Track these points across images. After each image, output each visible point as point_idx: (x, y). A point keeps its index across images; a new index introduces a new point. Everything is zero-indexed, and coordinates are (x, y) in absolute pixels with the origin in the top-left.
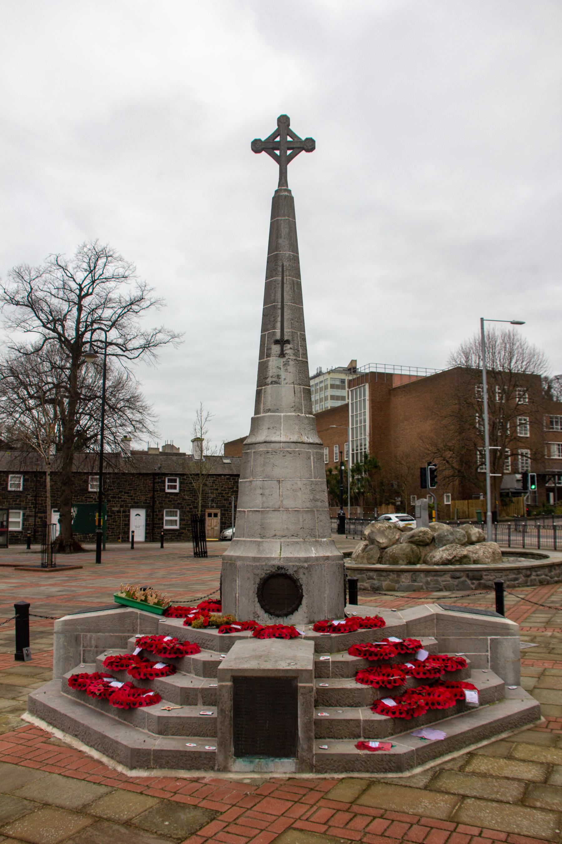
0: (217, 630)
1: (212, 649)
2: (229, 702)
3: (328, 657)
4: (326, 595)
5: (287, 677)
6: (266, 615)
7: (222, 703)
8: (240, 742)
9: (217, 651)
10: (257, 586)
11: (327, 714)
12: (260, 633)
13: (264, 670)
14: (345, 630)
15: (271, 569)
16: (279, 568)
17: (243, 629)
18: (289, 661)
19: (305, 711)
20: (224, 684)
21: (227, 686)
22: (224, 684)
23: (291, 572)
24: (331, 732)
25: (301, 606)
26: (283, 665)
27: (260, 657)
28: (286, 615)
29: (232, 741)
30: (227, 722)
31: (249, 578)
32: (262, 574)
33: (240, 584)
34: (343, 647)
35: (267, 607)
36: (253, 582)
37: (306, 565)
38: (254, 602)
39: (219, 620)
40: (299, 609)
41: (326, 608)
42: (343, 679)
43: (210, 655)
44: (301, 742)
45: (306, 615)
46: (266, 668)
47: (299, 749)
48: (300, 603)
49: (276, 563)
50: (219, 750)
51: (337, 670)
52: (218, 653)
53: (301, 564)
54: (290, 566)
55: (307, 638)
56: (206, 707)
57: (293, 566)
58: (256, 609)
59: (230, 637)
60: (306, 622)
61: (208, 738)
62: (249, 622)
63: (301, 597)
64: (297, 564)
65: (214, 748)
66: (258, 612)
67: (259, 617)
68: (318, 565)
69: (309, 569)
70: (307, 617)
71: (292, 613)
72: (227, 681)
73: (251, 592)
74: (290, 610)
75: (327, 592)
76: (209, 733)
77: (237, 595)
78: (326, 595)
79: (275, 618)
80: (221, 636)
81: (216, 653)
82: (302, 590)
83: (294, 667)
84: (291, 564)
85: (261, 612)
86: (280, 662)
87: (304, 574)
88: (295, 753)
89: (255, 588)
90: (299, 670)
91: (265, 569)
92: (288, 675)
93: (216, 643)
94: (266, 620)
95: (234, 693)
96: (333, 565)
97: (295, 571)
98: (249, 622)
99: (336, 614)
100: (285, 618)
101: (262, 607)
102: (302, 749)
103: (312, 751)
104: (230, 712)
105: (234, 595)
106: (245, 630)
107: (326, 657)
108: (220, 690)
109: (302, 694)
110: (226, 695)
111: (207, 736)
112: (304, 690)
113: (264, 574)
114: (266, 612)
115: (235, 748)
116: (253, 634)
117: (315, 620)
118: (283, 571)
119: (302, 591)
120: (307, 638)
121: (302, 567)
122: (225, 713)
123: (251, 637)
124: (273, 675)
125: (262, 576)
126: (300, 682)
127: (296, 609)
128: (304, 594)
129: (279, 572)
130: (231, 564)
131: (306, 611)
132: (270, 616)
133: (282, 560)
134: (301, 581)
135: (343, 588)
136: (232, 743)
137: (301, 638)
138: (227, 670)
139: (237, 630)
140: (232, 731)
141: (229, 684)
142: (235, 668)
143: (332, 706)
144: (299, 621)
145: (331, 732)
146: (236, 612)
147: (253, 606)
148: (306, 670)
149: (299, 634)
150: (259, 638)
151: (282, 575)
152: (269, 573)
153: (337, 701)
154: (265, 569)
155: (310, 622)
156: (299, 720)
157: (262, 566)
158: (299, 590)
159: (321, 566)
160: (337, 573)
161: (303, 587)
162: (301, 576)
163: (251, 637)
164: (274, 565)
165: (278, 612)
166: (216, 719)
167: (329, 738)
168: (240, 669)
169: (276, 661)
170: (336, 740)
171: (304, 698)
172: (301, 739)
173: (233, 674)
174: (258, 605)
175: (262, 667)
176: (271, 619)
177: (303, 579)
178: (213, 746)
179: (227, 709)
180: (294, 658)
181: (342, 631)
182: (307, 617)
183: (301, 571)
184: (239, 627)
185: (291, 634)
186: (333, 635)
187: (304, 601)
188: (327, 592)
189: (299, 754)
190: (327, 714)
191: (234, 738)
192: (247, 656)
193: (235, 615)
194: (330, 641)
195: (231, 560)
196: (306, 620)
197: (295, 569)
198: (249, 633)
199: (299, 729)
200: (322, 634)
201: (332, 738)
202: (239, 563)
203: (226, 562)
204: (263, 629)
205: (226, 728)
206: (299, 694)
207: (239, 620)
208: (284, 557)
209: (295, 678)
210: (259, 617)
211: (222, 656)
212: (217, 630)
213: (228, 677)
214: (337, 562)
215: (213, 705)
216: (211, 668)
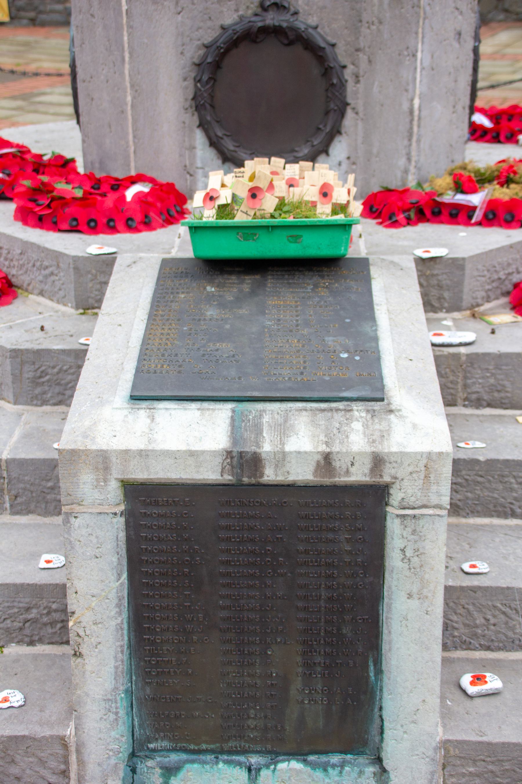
33: (427, 63)
77: (416, 102)
105: (406, 106)
146: (409, 160)
151: (276, 31)
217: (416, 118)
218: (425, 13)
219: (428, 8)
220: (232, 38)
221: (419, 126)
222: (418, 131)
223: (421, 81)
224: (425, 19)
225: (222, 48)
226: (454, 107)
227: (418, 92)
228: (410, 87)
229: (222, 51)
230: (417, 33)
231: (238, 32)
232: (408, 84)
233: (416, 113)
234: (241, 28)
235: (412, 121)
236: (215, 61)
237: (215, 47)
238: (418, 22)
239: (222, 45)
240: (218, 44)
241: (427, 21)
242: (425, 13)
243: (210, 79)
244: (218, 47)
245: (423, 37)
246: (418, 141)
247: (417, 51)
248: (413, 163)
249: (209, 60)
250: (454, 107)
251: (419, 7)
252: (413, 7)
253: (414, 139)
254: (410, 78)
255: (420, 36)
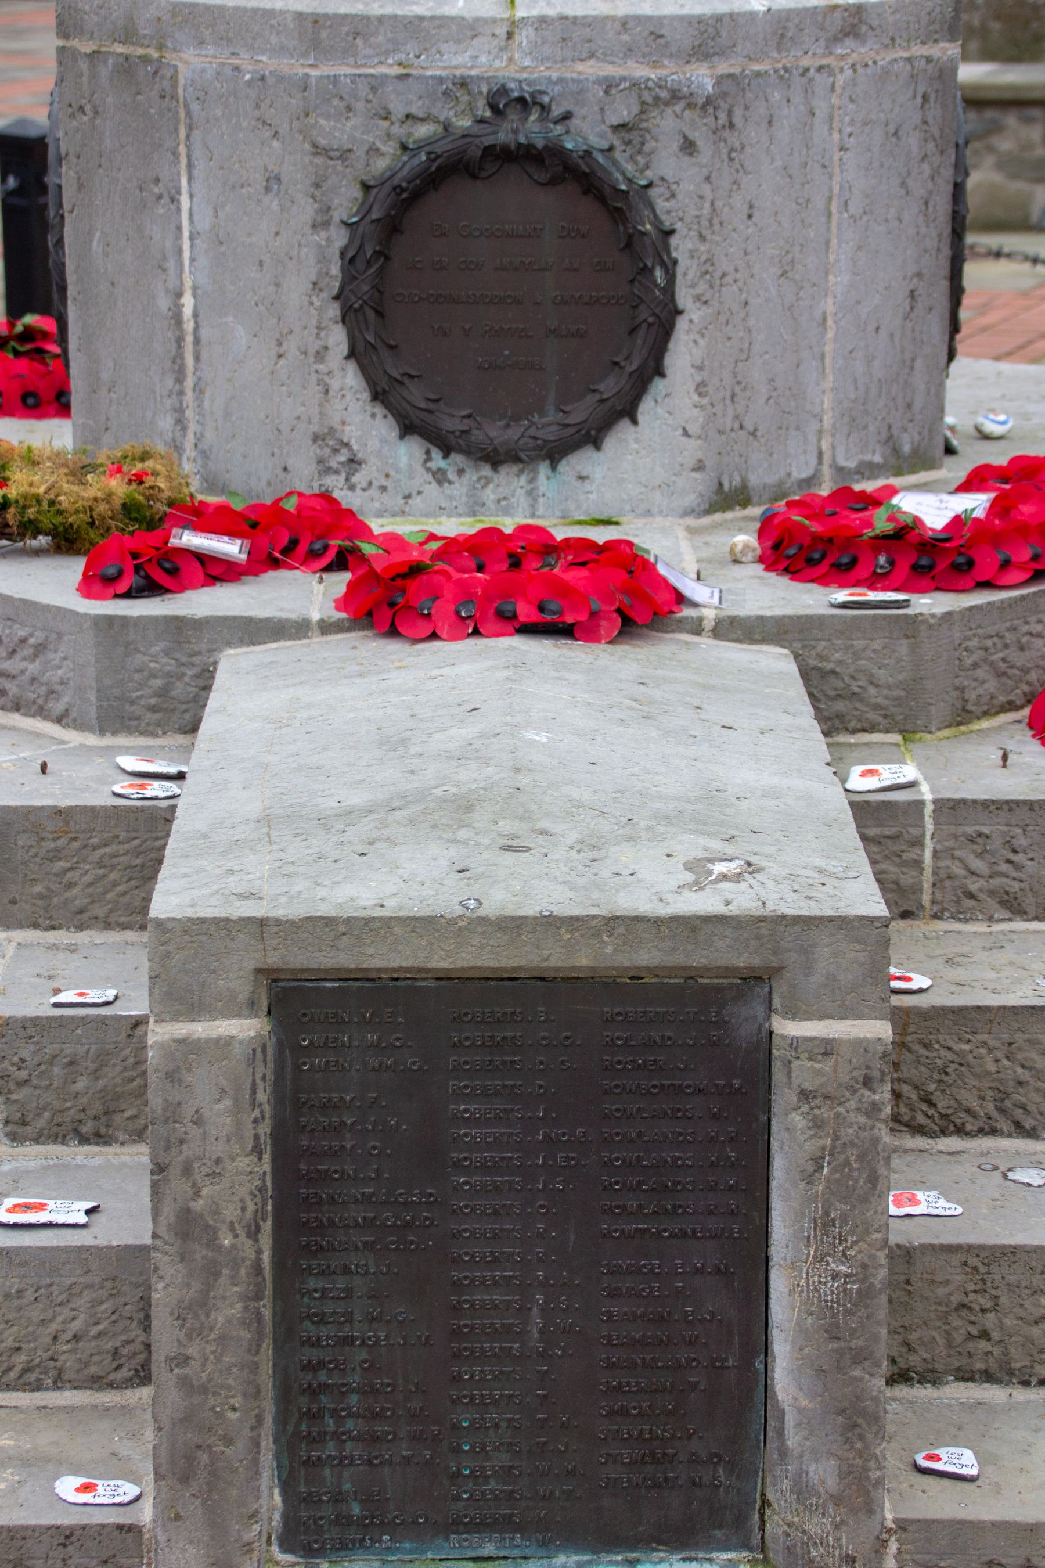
0: (74, 568)
1: (41, 712)
2: (244, 1163)
3: (909, 772)
4: (829, 306)
5: (690, 975)
6: (408, 453)
7: (187, 1171)
8: (331, 1449)
9: (81, 726)
10: (340, 238)
11: (943, 1206)
12: (394, 598)
13: (513, 926)
14: (1006, 565)
15: (445, 112)
16: (505, 102)
17: (262, 562)
18: (690, 845)
19: (826, 1223)
20: (200, 1029)
21: (224, 1044)
22: (200, 1029)
23: (587, 133)
24: (985, 1335)
25: (659, 386)
26: (655, 883)
27: (464, 806)
28: (554, 454)
29: (267, 1443)
30: (229, 1309)
31: (273, 181)
32: (373, 151)
33: (204, 223)
34: (991, 685)
35: (416, 394)
36: (306, 211)
37: (702, 78)
38: (321, 355)
39: (75, 496)
40: (646, 408)
41: (825, 397)
42: (1019, 925)
43: (34, 755)
44: (793, 1440)
45: (692, 450)
46: (530, 910)
47: (779, 1492)
48: (654, 367)
49: (484, 62)
50: (171, 1514)
51: (977, 864)
52: (92, 740)
53: (672, 72)
54: (580, 90)
55: (736, 629)
56: (33, 1156)
57: (609, 86)
58: (337, 405)
59: (179, 627)
60: (690, 499)
61: (68, 1397)
62: (290, 505)
63: (664, 321)
64: (641, 72)
65: (129, 1490)
66: (351, 433)
67: (354, 463)
68: (784, 77)
69: (719, 108)
70: (700, 467)
71: (593, 437)
72: (228, 1015)
73: (296, 288)
74: (580, 412)
75: (839, 280)
76: (69, 1363)
77: (188, 302)
78: (829, 306)
79: (471, 476)
80: (110, 621)
81: (74, 737)
82: (670, 268)
83: (742, 899)
84: (590, 70)
85: (370, 430)
86: (623, 857)
87: (689, 147)
88: (740, 1521)
89: (322, 259)
90: (782, 920)
91: (399, 110)
92: (699, 959)
93: (74, 665)
94: (417, 501)
95: (279, 1098)
96: (886, 74)
97: (621, 127)
98: (290, 505)
99: (891, 442)
100: (544, 468)
101: (378, 395)
102: (802, 1490)
103: (871, 1508)
104: (254, 1233)
105: (163, 303)
106: (275, 564)
107: (890, 774)
108: (172, 1076)
109: (805, 1095)
110: (220, 1114)
111: (59, 1383)
112: (826, 1066)
113: (390, 148)
114: (408, 428)
115: (287, 1486)
116: (344, 603)
117: (754, 480)
118: (532, 130)
119: (671, 278)
120: (736, 629)
121: (675, 96)
122: (212, 1242)
123: (326, 628)
124: (583, 960)
125: (381, 165)
126: (793, 1013)
127: (627, 410)
128: (684, 297)
129: (502, 136)
130: (127, 68)
131: (696, 420)
132: (438, 461)
133: (524, 37)
134: (662, 205)
135: (947, 252)
136: (267, 1458)
137: (696, 628)
138: (224, 925)
139: (217, 571)
140: (267, 1369)
141: (246, 1028)
142: (281, 911)
143: (960, 1131)
144: (634, 490)
145: (985, 1335)
146: (181, 423)
147: (314, 391)
148: (842, 923)
149: (680, 599)
150: (393, 632)
152: (429, 142)
153: (1001, 1096)
154: (399, 110)
155: (727, 498)
156: (779, 1283)
157: (376, 84)
158: (646, 271)
159: (808, 90)
160: (912, 141)
161: (681, 247)
162: (666, 163)
163: (326, 628)
164: (463, 83)
165: (495, 432)
166: (133, 1256)
167: (966, 1376)
168: (328, 922)
169: (593, 846)
170: (1021, 1394)
171: (818, 1124)
172: (790, 1420)
173: (273, 960)
174: (350, 379)
175: (499, 901)
176: (440, 477)
177: (679, 186)
178: (119, 1468)
179: (230, 1212)
180: (707, 810)
181: (981, 573)
182: (700, 467)
183: (667, 124)
184: (231, 548)
185: (609, 597)
186: (929, 604)
187: (683, 353)
188: (839, 280)
189: (775, 1527)
190: (943, 1206)
191: (282, 1419)
192: (357, 798)
193: (178, 449)
194: (903, 648)
195: (129, 35)
196: (694, 488)
197: (623, 111)
198: (309, 593)
199: (782, 1348)
200: (842, 595)
201: (989, 1377)
202: (191, 62)
203: (87, 47)
204: (415, 570)
205: (221, 1334)
206: (783, 1098)
207: (211, 484)
208: (543, 21)
209: (755, 982)
210: (354, 463)
211: (130, 763)
212: (74, 568)
213: (237, 974)
214: (919, 50)
215: (84, 1140)
216: (56, 855)
217: (189, 339)
218: (189, 114)
219: (195, 107)
220: (426, 170)
221: (197, 358)
222: (196, 369)
223: (193, 260)
224: (190, 128)
225: (403, 190)
226: (280, 344)
227: (188, 282)
228: (171, 264)
229: (405, 195)
230: (175, 154)
231: (438, 157)
232: (165, 258)
233: (189, 326)
234: (449, 147)
235: (180, 340)
236: (388, 216)
237: (387, 188)
238: (176, 130)
239: (404, 185)
240: (396, 181)
241: (196, 134)
242: (189, 114)
243: (377, 254)
244: (394, 189)
245: (190, 166)
246: (199, 390)
247: (179, 193)
248: (190, 436)
249: (375, 215)
250: (280, 344)
251: (174, 97)
252: (163, 97)
253: (189, 382)
254: (168, 244)
255: (184, 161)
